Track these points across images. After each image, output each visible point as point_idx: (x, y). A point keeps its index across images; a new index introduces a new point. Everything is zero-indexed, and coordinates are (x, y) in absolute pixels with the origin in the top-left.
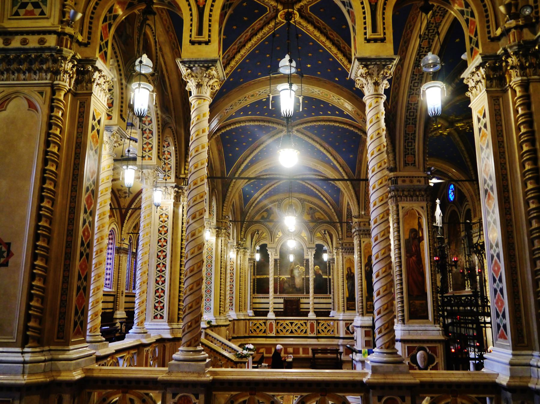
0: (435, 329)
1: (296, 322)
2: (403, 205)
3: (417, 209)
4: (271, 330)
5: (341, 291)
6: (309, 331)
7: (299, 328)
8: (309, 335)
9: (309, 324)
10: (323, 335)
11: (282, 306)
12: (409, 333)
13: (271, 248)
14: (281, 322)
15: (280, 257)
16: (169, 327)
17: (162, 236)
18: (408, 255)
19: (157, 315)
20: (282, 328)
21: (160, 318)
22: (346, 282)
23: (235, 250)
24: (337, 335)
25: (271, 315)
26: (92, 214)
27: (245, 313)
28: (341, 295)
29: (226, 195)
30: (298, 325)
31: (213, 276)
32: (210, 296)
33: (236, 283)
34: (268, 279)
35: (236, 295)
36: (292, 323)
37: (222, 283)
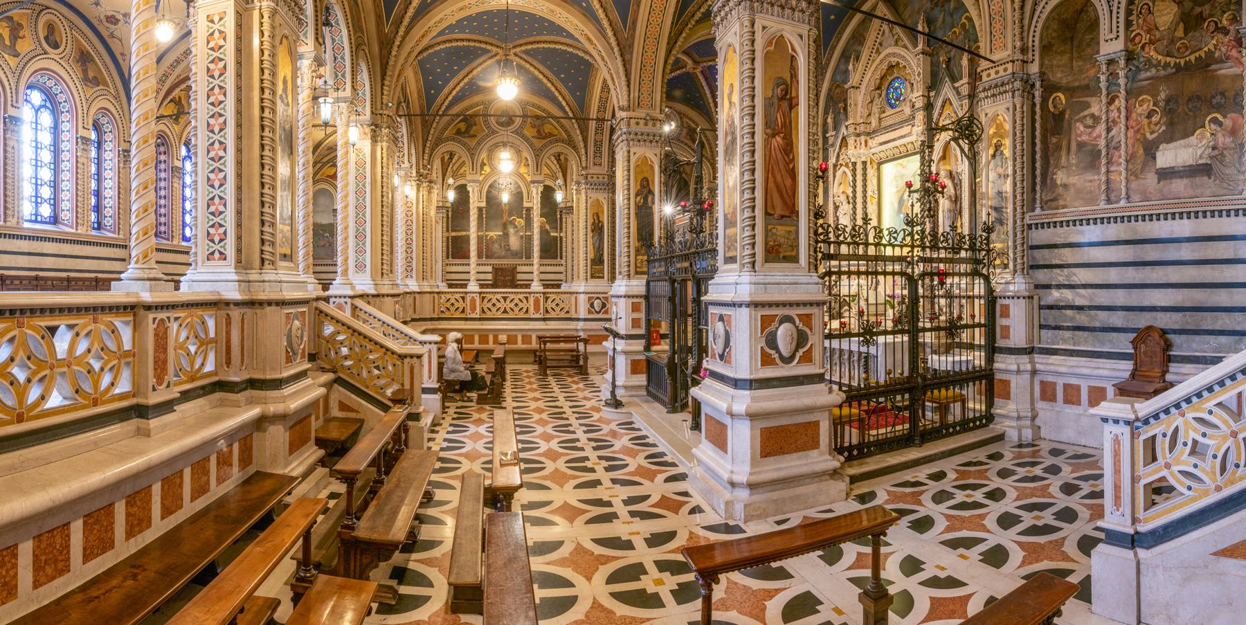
0: (811, 281)
1: (512, 296)
2: (766, 23)
3: (792, 39)
4: (473, 309)
5: (582, 250)
6: (532, 310)
7: (516, 305)
8: (532, 316)
9: (532, 300)
10: (553, 315)
11: (490, 276)
12: (766, 288)
13: (473, 181)
14: (489, 296)
15: (487, 202)
16: (236, 278)
17: (216, 82)
18: (768, 131)
19: (212, 253)
20: (490, 305)
21: (220, 259)
22: (590, 234)
23: (414, 183)
24: (574, 316)
25: (473, 287)
26: (273, 206)
27: (432, 282)
28: (582, 256)
29: (387, 63)
30: (515, 301)
31: (368, 210)
32: (364, 244)
33: (417, 237)
34: (468, 237)
35: (417, 255)
36: (505, 298)
37: (385, 223)
